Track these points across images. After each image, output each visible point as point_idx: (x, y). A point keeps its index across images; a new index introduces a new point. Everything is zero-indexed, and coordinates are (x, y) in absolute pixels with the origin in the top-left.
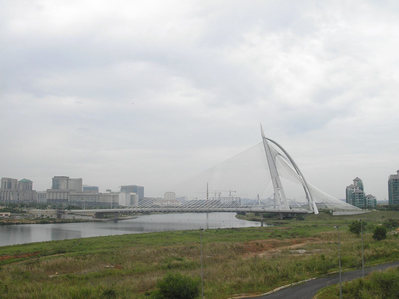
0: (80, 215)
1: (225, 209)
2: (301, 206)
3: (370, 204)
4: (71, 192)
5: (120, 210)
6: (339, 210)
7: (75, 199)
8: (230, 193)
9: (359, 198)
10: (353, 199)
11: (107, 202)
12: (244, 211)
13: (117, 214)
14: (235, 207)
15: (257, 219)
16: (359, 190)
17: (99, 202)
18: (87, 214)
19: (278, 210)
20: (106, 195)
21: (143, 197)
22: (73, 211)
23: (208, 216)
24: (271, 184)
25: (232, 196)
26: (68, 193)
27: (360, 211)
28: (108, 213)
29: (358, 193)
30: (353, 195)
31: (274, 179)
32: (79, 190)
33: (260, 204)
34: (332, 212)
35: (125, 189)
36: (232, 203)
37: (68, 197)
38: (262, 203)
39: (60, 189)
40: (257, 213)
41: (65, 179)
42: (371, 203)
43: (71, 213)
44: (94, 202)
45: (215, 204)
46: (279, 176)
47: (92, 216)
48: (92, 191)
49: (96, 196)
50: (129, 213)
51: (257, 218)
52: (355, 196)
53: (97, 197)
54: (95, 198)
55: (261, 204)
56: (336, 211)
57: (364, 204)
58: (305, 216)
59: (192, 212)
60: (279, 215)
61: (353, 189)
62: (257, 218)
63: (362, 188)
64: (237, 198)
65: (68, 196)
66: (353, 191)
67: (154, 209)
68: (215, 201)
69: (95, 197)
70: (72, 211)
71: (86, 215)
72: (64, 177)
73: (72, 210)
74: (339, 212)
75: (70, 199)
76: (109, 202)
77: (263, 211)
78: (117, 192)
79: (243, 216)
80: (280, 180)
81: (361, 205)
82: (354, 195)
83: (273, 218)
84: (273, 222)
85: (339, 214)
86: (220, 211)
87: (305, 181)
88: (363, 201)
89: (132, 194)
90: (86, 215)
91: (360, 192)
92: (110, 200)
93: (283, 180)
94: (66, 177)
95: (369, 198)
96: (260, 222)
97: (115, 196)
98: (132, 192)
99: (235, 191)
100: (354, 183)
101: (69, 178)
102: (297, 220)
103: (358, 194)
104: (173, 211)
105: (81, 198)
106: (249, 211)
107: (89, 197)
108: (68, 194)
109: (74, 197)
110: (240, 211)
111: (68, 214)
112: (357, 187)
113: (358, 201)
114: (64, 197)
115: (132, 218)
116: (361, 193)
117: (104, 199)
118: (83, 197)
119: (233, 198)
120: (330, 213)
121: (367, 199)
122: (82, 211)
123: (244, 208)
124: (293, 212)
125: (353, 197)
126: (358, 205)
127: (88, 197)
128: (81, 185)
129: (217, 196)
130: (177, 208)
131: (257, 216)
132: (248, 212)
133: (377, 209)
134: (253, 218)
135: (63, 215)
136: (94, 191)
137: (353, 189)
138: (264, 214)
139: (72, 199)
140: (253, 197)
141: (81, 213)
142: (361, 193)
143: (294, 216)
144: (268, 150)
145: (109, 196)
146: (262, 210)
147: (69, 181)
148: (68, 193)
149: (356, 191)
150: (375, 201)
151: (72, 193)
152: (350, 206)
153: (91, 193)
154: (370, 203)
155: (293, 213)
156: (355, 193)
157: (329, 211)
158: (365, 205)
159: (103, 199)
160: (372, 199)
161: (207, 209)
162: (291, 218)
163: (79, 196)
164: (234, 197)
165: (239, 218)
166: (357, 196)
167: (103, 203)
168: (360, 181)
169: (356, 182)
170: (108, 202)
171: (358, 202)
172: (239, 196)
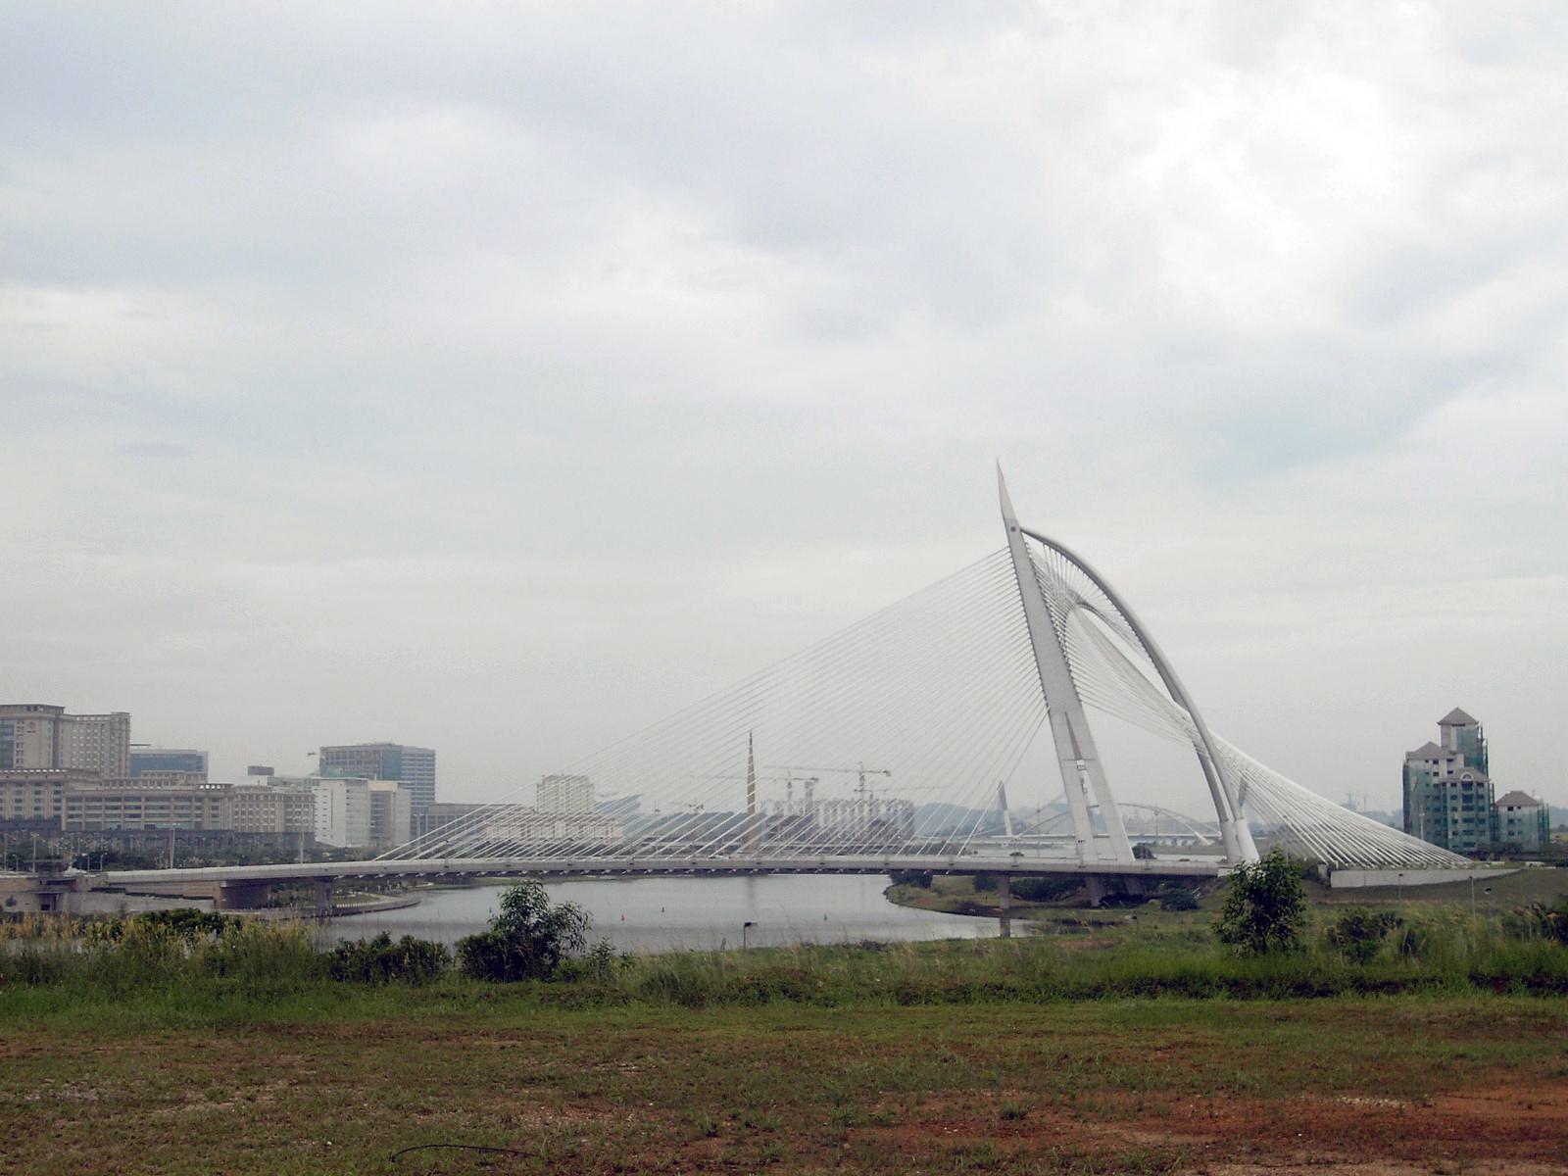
0: (151, 895)
1: (832, 859)
2: (1213, 842)
3: (1516, 838)
4: (75, 780)
5: (341, 868)
6: (1363, 864)
7: (98, 816)
8: (862, 778)
9: (1464, 809)
10: (1437, 810)
11: (254, 831)
12: (919, 867)
13: (328, 885)
14: (880, 847)
15: (984, 904)
16: (1461, 770)
17: (216, 832)
18: (186, 889)
19: (1078, 862)
20: (251, 796)
21: (433, 799)
22: (115, 875)
23: (752, 896)
24: (1044, 742)
25: (871, 796)
26: (58, 789)
27: (1460, 868)
28: (284, 885)
29: (1459, 785)
30: (1435, 793)
31: (1058, 719)
32: (112, 771)
33: (1010, 834)
34: (1329, 875)
35: (341, 761)
36: (871, 827)
37: (57, 809)
38: (1019, 827)
39: (15, 765)
40: (985, 878)
41: (40, 718)
42: (1520, 833)
43: (107, 886)
44: (193, 828)
45: (787, 836)
46: (1081, 706)
47: (211, 898)
48: (178, 777)
49: (200, 799)
50: (375, 882)
51: (984, 899)
52: (1445, 796)
53: (207, 804)
54: (198, 808)
55: (1015, 832)
56: (1346, 869)
57: (1488, 833)
58: (1204, 893)
59: (680, 872)
60: (1084, 886)
61: (1436, 762)
62: (984, 899)
63: (1480, 762)
64: (896, 805)
65: (58, 804)
66: (1436, 774)
67: (504, 860)
68: (791, 819)
69: (199, 804)
70: (113, 877)
71: (181, 896)
72: (36, 707)
73: (111, 874)
74: (1363, 872)
75: (71, 816)
76: (269, 830)
77: (1008, 868)
78: (305, 780)
79: (918, 889)
80: (1087, 725)
81: (1472, 839)
82: (1443, 793)
83: (1056, 900)
84: (1055, 917)
85: (1360, 884)
86: (811, 871)
87: (1203, 731)
88: (1482, 821)
89: (377, 785)
90: (181, 896)
91: (1470, 777)
92: (271, 820)
93: (1101, 724)
94: (47, 708)
95: (1510, 809)
96: (997, 920)
97: (297, 797)
98: (378, 779)
99: (885, 772)
100: (1445, 735)
101: (66, 712)
102: (1163, 908)
103: (1459, 790)
104: (593, 872)
105: (128, 812)
106: (944, 867)
107: (166, 803)
108: (57, 792)
109: (88, 808)
110: (900, 866)
111: (95, 890)
112: (1454, 753)
113: (1460, 821)
114: (37, 809)
115: (396, 904)
116: (1475, 784)
117: (243, 813)
118: (137, 804)
119: (873, 804)
120: (1318, 879)
121: (1503, 810)
122: (163, 876)
123: (922, 853)
124: (1148, 872)
125: (1437, 804)
126: (1457, 839)
127: (162, 808)
128: (123, 743)
129: (799, 791)
130: (610, 858)
131: (984, 893)
132: (942, 872)
133: (1549, 862)
134: (966, 900)
135: (66, 896)
136: (190, 775)
137: (1436, 762)
138: (1013, 880)
139: (78, 816)
140: (978, 799)
141: (142, 883)
142: (1475, 784)
143: (1155, 888)
144: (1031, 581)
145: (266, 796)
146: (1070, 865)
147: (64, 727)
148: (58, 789)
149: (1450, 772)
150: (1543, 818)
151: (80, 788)
152: (1418, 844)
153: (174, 788)
154: (1515, 829)
155: (1149, 879)
156: (1444, 784)
157: (1313, 867)
158: (1494, 838)
159: (237, 813)
160: (1526, 811)
161: (749, 859)
162: (1138, 900)
163: (118, 799)
164: (881, 798)
165: (900, 900)
166: (1454, 797)
167: (237, 834)
168: (1473, 727)
169: (1454, 731)
170: (263, 827)
171: (1461, 827)
172: (902, 796)
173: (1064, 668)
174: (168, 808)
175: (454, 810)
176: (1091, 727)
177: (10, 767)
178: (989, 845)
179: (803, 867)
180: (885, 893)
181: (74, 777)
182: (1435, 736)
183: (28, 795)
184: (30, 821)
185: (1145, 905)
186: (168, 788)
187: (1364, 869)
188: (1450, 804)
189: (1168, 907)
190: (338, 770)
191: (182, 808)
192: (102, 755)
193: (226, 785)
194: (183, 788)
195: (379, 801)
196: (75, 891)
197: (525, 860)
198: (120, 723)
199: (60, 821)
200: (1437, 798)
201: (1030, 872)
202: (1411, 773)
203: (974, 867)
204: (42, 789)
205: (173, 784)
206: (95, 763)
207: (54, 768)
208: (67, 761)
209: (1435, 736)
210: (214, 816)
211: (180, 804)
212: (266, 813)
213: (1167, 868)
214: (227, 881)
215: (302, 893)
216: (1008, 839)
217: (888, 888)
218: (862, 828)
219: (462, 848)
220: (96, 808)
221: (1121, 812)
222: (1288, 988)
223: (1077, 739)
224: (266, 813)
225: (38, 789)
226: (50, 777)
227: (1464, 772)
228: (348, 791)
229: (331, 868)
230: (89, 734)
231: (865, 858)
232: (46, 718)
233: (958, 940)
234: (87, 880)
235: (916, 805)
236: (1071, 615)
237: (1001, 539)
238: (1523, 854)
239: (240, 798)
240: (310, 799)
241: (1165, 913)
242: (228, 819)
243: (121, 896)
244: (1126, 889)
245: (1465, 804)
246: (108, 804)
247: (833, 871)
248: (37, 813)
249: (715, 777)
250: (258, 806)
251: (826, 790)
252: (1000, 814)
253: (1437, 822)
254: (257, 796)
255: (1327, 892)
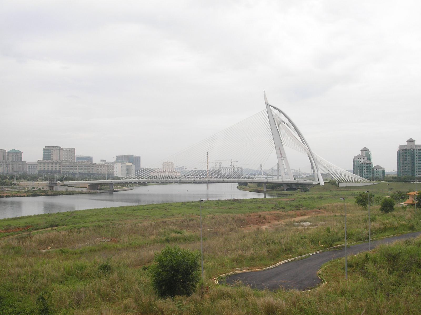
0: (73, 187)
1: (226, 179)
2: (306, 177)
3: (378, 176)
4: (64, 162)
7: (68, 170)
8: (232, 162)
9: (367, 169)
10: (361, 169)
12: (245, 181)
13: (112, 185)
18: (81, 186)
19: (282, 181)
22: (66, 182)
27: (368, 183)
29: (366, 164)
30: (360, 165)
33: (263, 175)
34: (338, 184)
35: (121, 159)
37: (60, 168)
38: (265, 173)
39: (51, 159)
40: (260, 184)
41: (56, 149)
44: (88, 172)
45: (215, 175)
49: (89, 166)
50: (125, 184)
51: (259, 189)
54: (89, 168)
56: (342, 182)
57: (372, 174)
59: (191, 182)
61: (360, 159)
62: (259, 189)
63: (370, 159)
64: (239, 168)
66: (361, 161)
68: (216, 171)
69: (89, 167)
72: (55, 147)
73: (64, 182)
75: (63, 170)
81: (368, 176)
83: (276, 189)
86: (221, 182)
88: (370, 172)
91: (368, 162)
92: (105, 171)
98: (128, 162)
100: (362, 153)
103: (365, 165)
109: (66, 168)
110: (241, 181)
112: (364, 157)
113: (365, 172)
114: (56, 168)
118: (76, 167)
119: (234, 168)
120: (336, 185)
121: (375, 170)
122: (76, 183)
123: (251, 178)
125: (360, 168)
127: (81, 168)
129: (218, 166)
131: (260, 187)
132: (251, 183)
133: (386, 181)
137: (360, 159)
143: (298, 187)
144: (272, 117)
145: (104, 166)
147: (61, 151)
149: (363, 161)
154: (377, 174)
155: (297, 184)
156: (362, 164)
159: (97, 169)
160: (380, 170)
162: (295, 189)
164: (236, 167)
165: (241, 189)
166: (364, 167)
167: (97, 174)
170: (103, 172)
171: (366, 173)
172: (240, 166)
173: (279, 136)
174: (83, 168)
175: (145, 170)
176: (285, 150)
177: (50, 159)
178: (258, 177)
179: (219, 181)
180: (237, 187)
181: (63, 162)
182: (360, 153)
183: (54, 165)
184: (51, 171)
185: (297, 190)
186: (83, 164)
187: (346, 182)
188: (363, 168)
189: (302, 191)
190: (120, 161)
191: (86, 168)
192: (69, 157)
193: (95, 164)
194: (86, 164)
195: (128, 167)
196: (57, 186)
197: (156, 179)
198: (73, 150)
199: (61, 171)
200: (361, 167)
201: (271, 183)
202: (355, 161)
203: (258, 182)
204: (45, 164)
205: (84, 163)
206: (68, 159)
207: (59, 160)
208: (62, 158)
209: (360, 153)
210: (92, 170)
211: (75, 167)
212: (104, 169)
213: (302, 182)
214: (90, 184)
215: (107, 187)
216: (262, 176)
217: (238, 186)
218: (231, 173)
219: (145, 177)
220: (68, 168)
221: (292, 171)
222: (207, 211)
223: (282, 153)
224: (104, 169)
225: (56, 164)
226: (47, 162)
227: (367, 161)
228: (121, 165)
229: (113, 181)
230: (67, 153)
231: (233, 179)
232: (57, 149)
233: (256, 198)
234: (59, 183)
235: (243, 168)
236: (280, 125)
237: (265, 107)
238: (380, 179)
239: (98, 166)
240: (113, 167)
241: (302, 192)
242: (95, 171)
243: (67, 187)
244: (292, 187)
245: (367, 168)
246: (70, 167)
247: (226, 182)
248: (56, 169)
249: (201, 162)
250: (102, 168)
251: (224, 165)
252: (261, 171)
253: (360, 172)
254: (102, 166)
255: (338, 188)
